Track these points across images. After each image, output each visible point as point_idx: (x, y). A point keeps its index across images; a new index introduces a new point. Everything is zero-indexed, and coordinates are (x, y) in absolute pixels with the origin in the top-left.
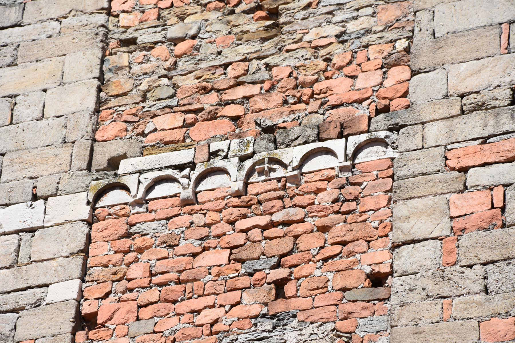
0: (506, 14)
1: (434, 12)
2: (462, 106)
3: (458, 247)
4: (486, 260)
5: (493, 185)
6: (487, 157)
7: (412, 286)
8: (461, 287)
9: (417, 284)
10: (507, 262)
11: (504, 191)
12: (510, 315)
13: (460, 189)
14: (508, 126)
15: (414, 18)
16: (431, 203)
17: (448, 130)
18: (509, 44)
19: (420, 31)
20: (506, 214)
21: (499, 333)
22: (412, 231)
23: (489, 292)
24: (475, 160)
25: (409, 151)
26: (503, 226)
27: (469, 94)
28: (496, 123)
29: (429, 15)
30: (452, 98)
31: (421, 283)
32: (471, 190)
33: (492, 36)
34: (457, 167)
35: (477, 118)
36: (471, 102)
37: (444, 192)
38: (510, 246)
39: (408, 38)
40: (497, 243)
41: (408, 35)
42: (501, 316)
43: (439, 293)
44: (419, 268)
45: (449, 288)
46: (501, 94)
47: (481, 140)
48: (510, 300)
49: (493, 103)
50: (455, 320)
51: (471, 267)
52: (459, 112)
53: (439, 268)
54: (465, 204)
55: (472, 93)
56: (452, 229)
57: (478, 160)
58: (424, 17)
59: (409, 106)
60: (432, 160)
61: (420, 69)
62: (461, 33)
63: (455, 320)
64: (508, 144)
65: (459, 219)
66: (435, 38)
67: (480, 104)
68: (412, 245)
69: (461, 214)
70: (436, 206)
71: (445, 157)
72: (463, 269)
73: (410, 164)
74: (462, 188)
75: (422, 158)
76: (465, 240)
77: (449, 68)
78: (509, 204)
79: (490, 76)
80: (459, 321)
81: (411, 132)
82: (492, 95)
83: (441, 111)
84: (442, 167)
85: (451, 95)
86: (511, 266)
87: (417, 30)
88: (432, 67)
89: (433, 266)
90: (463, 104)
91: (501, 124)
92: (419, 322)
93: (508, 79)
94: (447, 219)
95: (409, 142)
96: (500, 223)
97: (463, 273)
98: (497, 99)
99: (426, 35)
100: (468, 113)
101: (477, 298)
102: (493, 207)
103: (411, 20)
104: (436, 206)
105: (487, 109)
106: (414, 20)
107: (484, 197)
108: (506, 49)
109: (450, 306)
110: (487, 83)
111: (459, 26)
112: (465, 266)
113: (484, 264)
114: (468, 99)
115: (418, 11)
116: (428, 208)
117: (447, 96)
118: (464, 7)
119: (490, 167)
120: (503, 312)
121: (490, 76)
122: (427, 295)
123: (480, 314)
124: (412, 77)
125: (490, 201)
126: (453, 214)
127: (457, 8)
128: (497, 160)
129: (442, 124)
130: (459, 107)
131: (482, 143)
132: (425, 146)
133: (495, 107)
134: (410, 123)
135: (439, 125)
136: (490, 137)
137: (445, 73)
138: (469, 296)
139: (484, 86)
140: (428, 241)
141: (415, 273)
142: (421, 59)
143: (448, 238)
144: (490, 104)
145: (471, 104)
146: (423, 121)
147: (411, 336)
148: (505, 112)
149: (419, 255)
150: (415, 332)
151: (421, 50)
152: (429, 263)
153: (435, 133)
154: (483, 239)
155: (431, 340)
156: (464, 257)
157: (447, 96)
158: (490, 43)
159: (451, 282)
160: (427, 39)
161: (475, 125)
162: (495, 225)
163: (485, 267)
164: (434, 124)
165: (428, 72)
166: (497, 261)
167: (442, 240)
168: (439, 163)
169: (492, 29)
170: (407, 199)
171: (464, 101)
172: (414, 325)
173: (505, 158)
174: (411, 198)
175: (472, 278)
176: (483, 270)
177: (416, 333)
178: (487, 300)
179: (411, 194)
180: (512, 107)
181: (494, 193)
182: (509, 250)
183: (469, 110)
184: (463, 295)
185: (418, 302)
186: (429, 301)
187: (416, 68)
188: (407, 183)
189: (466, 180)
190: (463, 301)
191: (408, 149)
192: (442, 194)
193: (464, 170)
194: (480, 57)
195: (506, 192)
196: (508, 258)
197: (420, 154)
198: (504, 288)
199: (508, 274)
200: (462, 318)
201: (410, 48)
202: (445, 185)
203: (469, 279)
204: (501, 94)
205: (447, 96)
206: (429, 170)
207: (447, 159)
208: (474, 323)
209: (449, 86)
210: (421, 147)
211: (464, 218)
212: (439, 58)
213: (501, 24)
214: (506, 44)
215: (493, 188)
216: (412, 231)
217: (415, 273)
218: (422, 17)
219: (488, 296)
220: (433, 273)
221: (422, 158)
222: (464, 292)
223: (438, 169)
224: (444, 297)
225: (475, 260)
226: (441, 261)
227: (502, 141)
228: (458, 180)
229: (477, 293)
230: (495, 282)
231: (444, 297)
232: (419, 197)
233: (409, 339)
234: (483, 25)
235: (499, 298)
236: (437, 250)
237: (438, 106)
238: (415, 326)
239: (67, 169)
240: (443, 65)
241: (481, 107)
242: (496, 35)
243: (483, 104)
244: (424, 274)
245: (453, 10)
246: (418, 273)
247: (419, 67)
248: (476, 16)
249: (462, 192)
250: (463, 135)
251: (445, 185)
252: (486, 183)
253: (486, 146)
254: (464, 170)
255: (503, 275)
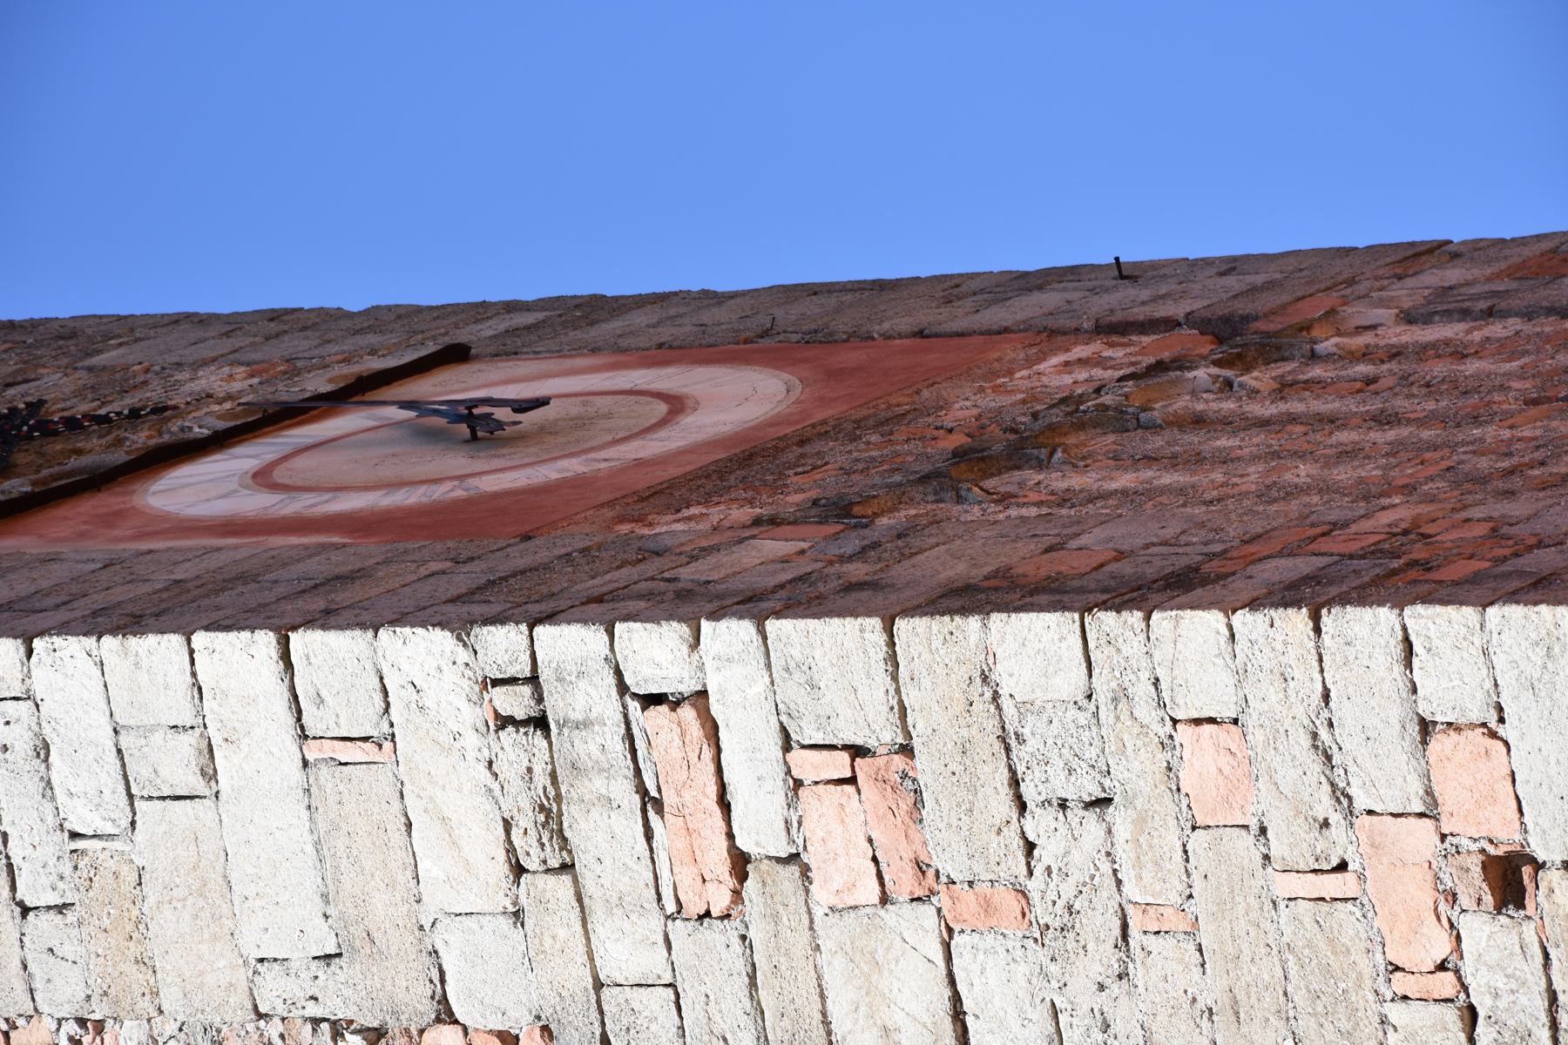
0: (274, 750)
1: (261, 960)
2: (548, 871)
3: (971, 883)
4: (1008, 802)
5: (785, 781)
6: (700, 797)
7: (1092, 1022)
8: (1092, 877)
9: (1086, 1008)
10: (1013, 743)
11: (803, 747)
12: (1171, 737)
13: (798, 874)
14: (608, 737)
15: (277, 1020)
16: (839, 962)
17: (618, 912)
18: (365, 739)
19: (316, 999)
20: (871, 743)
21: (1227, 770)
22: (926, 1018)
23: (1103, 795)
24: (709, 832)
25: (682, 1028)
26: (907, 750)
27: (511, 850)
28: (601, 770)
29: (270, 973)
30: (523, 900)
31: (1081, 997)
32: (800, 842)
33: (341, 788)
34: (732, 883)
35: (583, 827)
36: (535, 844)
37: (806, 922)
38: (965, 732)
39: (337, 1034)
40: (959, 769)
41: (328, 1036)
42: (1175, 763)
43: (1112, 942)
44: (1038, 1000)
45: (1098, 913)
46: (513, 757)
47: (651, 814)
48: (1126, 737)
49: (541, 779)
50: (1190, 896)
51: (1030, 847)
52: (566, 879)
53: (1036, 940)
54: (841, 861)
55: (510, 842)
56: (919, 899)
57: (709, 821)
58: (273, 990)
59: (545, 1029)
60: (709, 958)
61: (433, 998)
62: (329, 875)
63: (1190, 896)
64: (662, 735)
65: (887, 878)
66: (339, 955)
67: (542, 818)
68: (969, 1020)
69: (874, 871)
70: (848, 948)
71: (701, 918)
72: (1039, 871)
73: (723, 1025)
74: (794, 870)
75: (703, 989)
76: (949, 863)
77: (432, 909)
78: (841, 735)
79: (460, 791)
80: (1195, 884)
81: (625, 1022)
82: (516, 785)
83: (562, 933)
84: (732, 929)
85: (515, 904)
86: (1026, 732)
87: (313, 1010)
88: (427, 961)
89: (1031, 958)
90: (542, 868)
91: (603, 758)
92: (1201, 1005)
93: (471, 740)
94: (889, 915)
95: (653, 1027)
96: (899, 761)
97: (1049, 869)
98: (529, 770)
99: (330, 982)
100: (570, 852)
101: (1122, 831)
102: (852, 780)
103: (281, 1028)
104: (848, 948)
105: (558, 798)
106: (283, 1019)
107: (821, 807)
108: (380, 746)
109: (1151, 910)
110: (480, 799)
111: (308, 883)
112: (1028, 864)
113: (1022, 807)
114: (528, 854)
115: (256, 1007)
116: (857, 971)
117: (516, 914)
118: (250, 870)
119: (730, 789)
120: (1162, 757)
121: (460, 791)
122: (1120, 977)
123: (1172, 822)
124: (456, 1022)
125: (831, 787)
126: (875, 897)
127: (251, 890)
128: (711, 768)
129: (599, 929)
130: (552, 880)
131: (660, 811)
132: (668, 979)
133: (553, 776)
134: (597, 1024)
135: (602, 937)
136: (642, 791)
137: (448, 920)
138: (1121, 852)
139: (488, 807)
140: (955, 970)
141: (1055, 1012)
142: (401, 996)
143: (945, 912)
144: (545, 788)
145: (542, 845)
146: (590, 987)
147: (1244, 1029)
148: (568, 745)
149: (997, 999)
150: (1233, 1018)
151: (374, 995)
152: (1022, 970)
153: (628, 950)
154: (946, 811)
155: (1254, 970)
156: (1003, 865)
157: (518, 916)
158: (361, 793)
159: (1077, 906)
160: (342, 977)
161: (604, 831)
162: (905, 776)
163: (1030, 805)
164: (602, 952)
165: (442, 973)
166: (1012, 771)
167: (950, 930)
168: (715, 934)
169: (320, 787)
170: (829, 1033)
171: (531, 864)
172: (1210, 1019)
173: (705, 747)
174: (826, 1023)
175: (1063, 844)
176: (1038, 811)
177: (1237, 1014)
178: (1129, 802)
179: (814, 1023)
180: (553, 726)
181: (807, 776)
182: (979, 736)
183: (561, 850)
184: (1115, 871)
185: (1141, 1005)
186: (1137, 972)
187: (429, 1010)
188: (779, 1034)
189: (770, 858)
190: (1132, 873)
191: (675, 1030)
192: (811, 928)
193: (740, 863)
194: (403, 820)
195: (806, 742)
196: (1003, 739)
197: (691, 994)
198: (1091, 753)
199: (1050, 742)
200: (1184, 877)
201: (369, 1029)
202: (785, 919)
203: (1067, 853)
204: (513, 757)
205: (518, 916)
206: (741, 966)
207: (708, 914)
208: (1198, 841)
209: (487, 909)
210: (670, 991)
211: (883, 866)
212: (399, 942)
213: (305, 763)
214: (367, 746)
215: (795, 780)
216: (926, 1018)
217: (1055, 1012)
218: (275, 993)
219: (1116, 799)
220: (1053, 959)
221: (703, 989)
222: (1106, 867)
223: (736, 942)
224: (1125, 927)
225: (1012, 833)
226: (1015, 931)
227: (655, 754)
228: (769, 881)
229: (1110, 832)
230: (1073, 779)
231: (1125, 927)
232: (823, 997)
233: (1255, 1037)
234: (305, 814)
235: (1121, 768)
236: (981, 945)
237: (548, 942)
238: (1215, 1018)
239: (687, 713)
240: (421, 928)
241: (551, 816)
242: (337, 774)
243: (542, 808)
244: (1055, 985)
245: (259, 903)
246: (1053, 1004)
247: (427, 1001)
248: (278, 834)
249: (805, 870)
250: (635, 867)
251: (785, 919)
252: (780, 799)
253: (669, 799)
254: (740, 863)
255: (1053, 755)
